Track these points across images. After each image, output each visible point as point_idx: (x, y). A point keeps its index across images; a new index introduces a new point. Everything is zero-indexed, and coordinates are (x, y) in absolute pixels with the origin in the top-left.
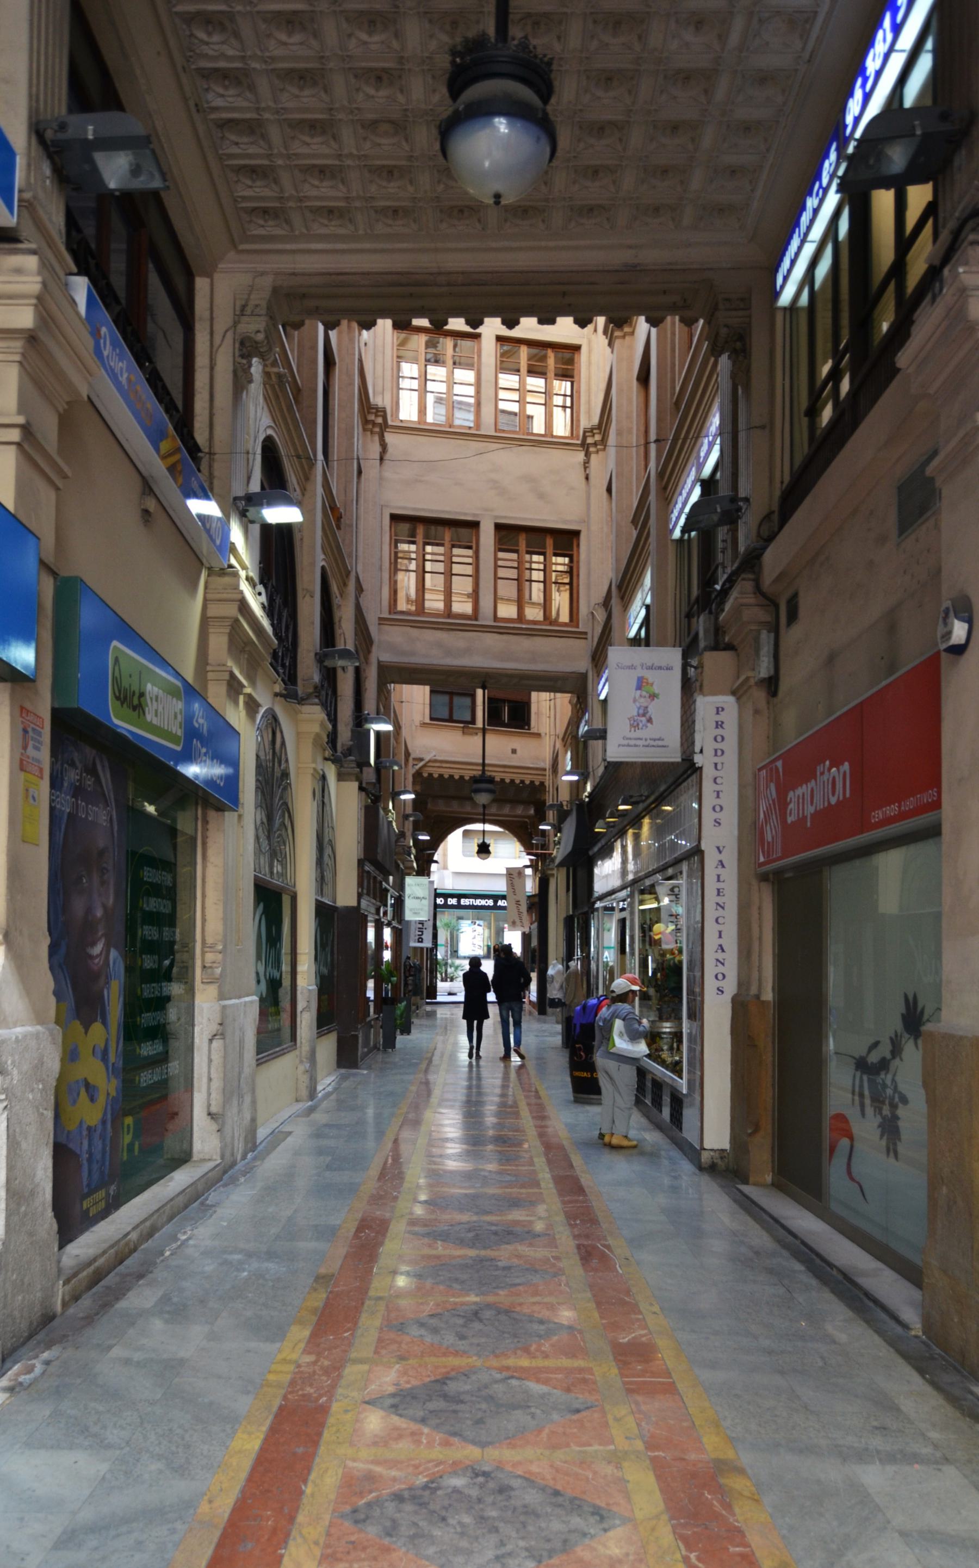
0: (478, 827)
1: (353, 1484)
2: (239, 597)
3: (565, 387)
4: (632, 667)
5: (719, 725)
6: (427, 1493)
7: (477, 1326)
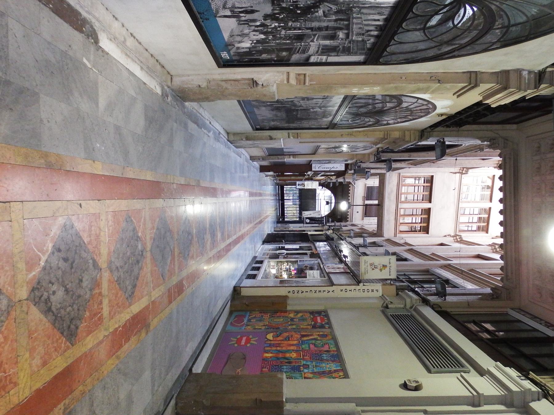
3: (475, 228)
4: (390, 263)
5: (373, 291)
6: (136, 238)
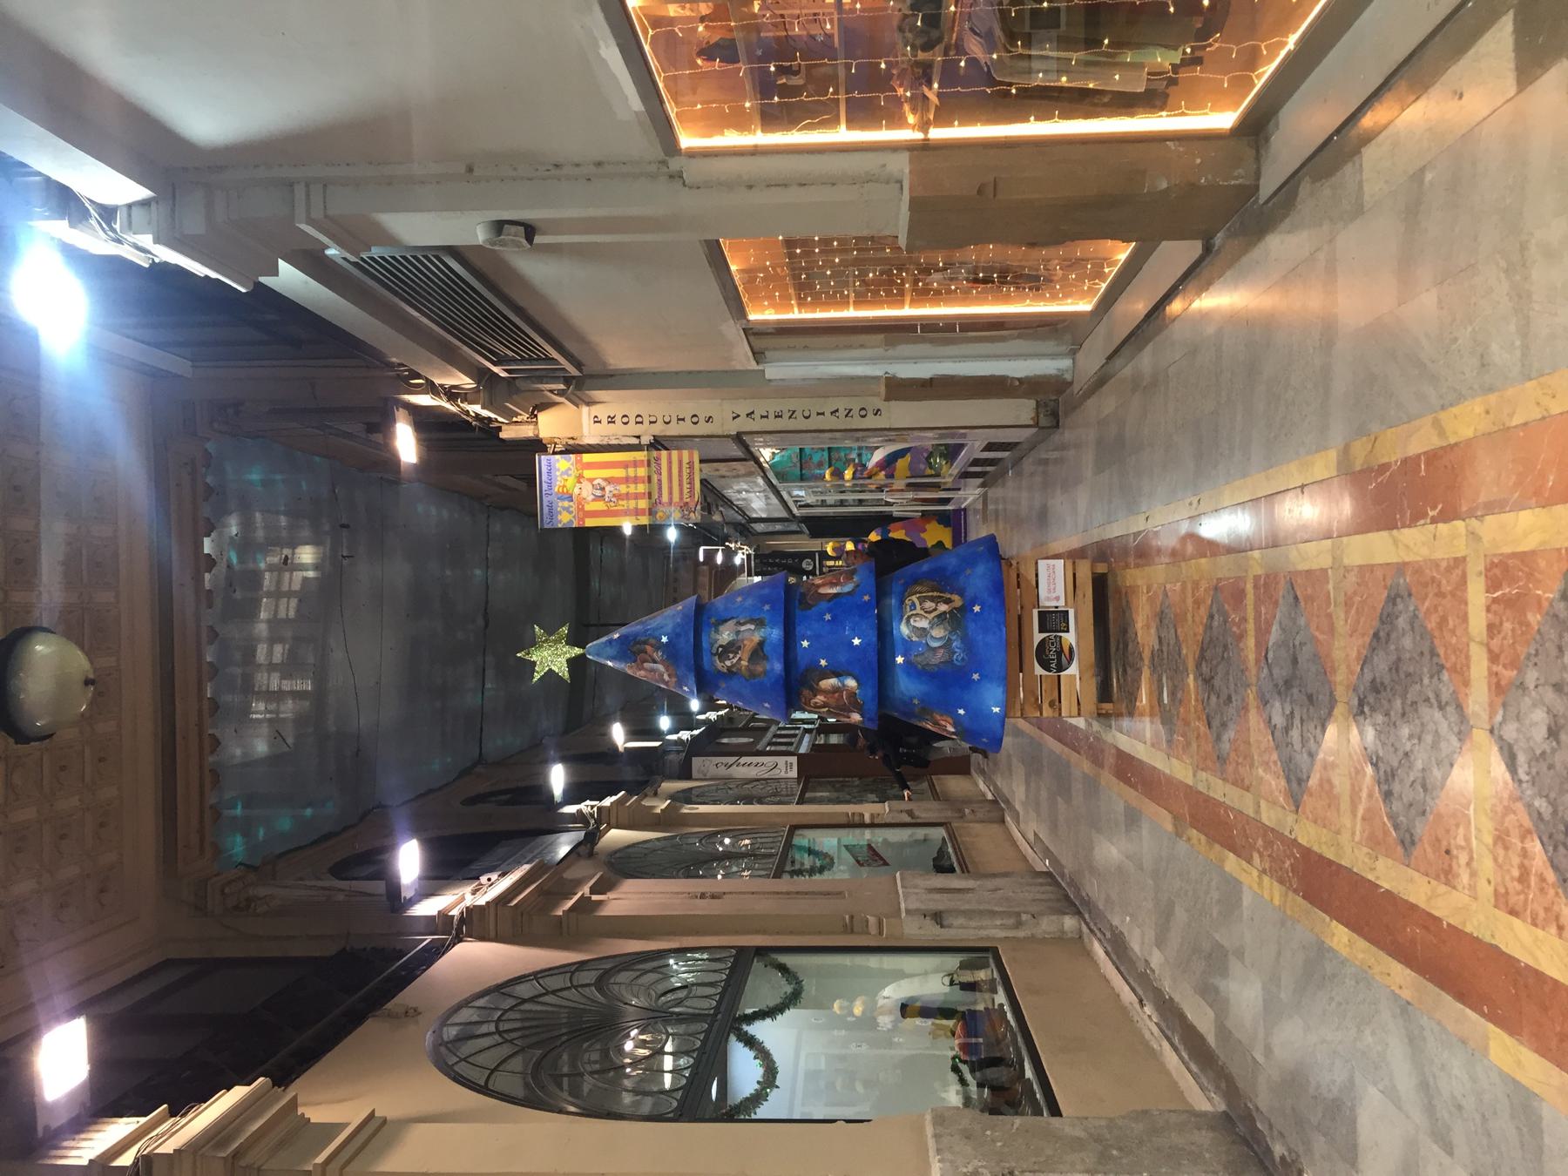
1: (1375, 843)
5: (611, 420)
7: (1217, 682)
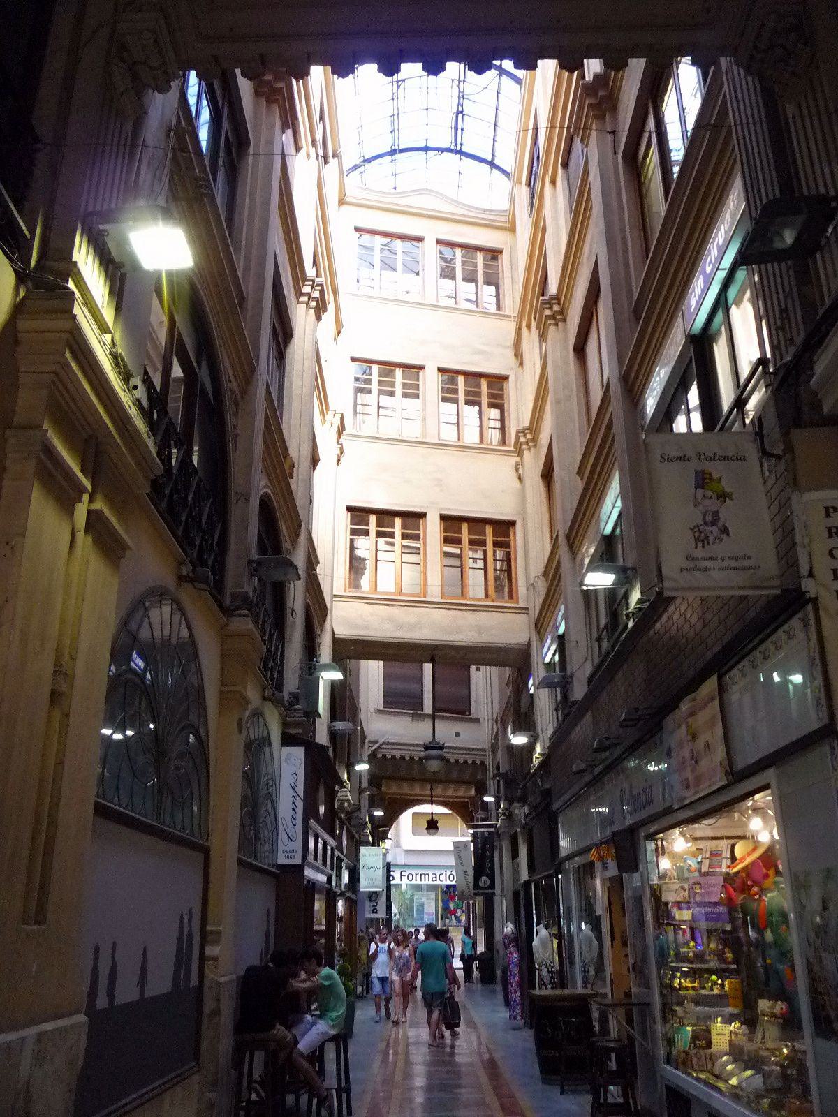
0: (425, 808)
2: (67, 325)
3: (495, 413)
4: (683, 459)
